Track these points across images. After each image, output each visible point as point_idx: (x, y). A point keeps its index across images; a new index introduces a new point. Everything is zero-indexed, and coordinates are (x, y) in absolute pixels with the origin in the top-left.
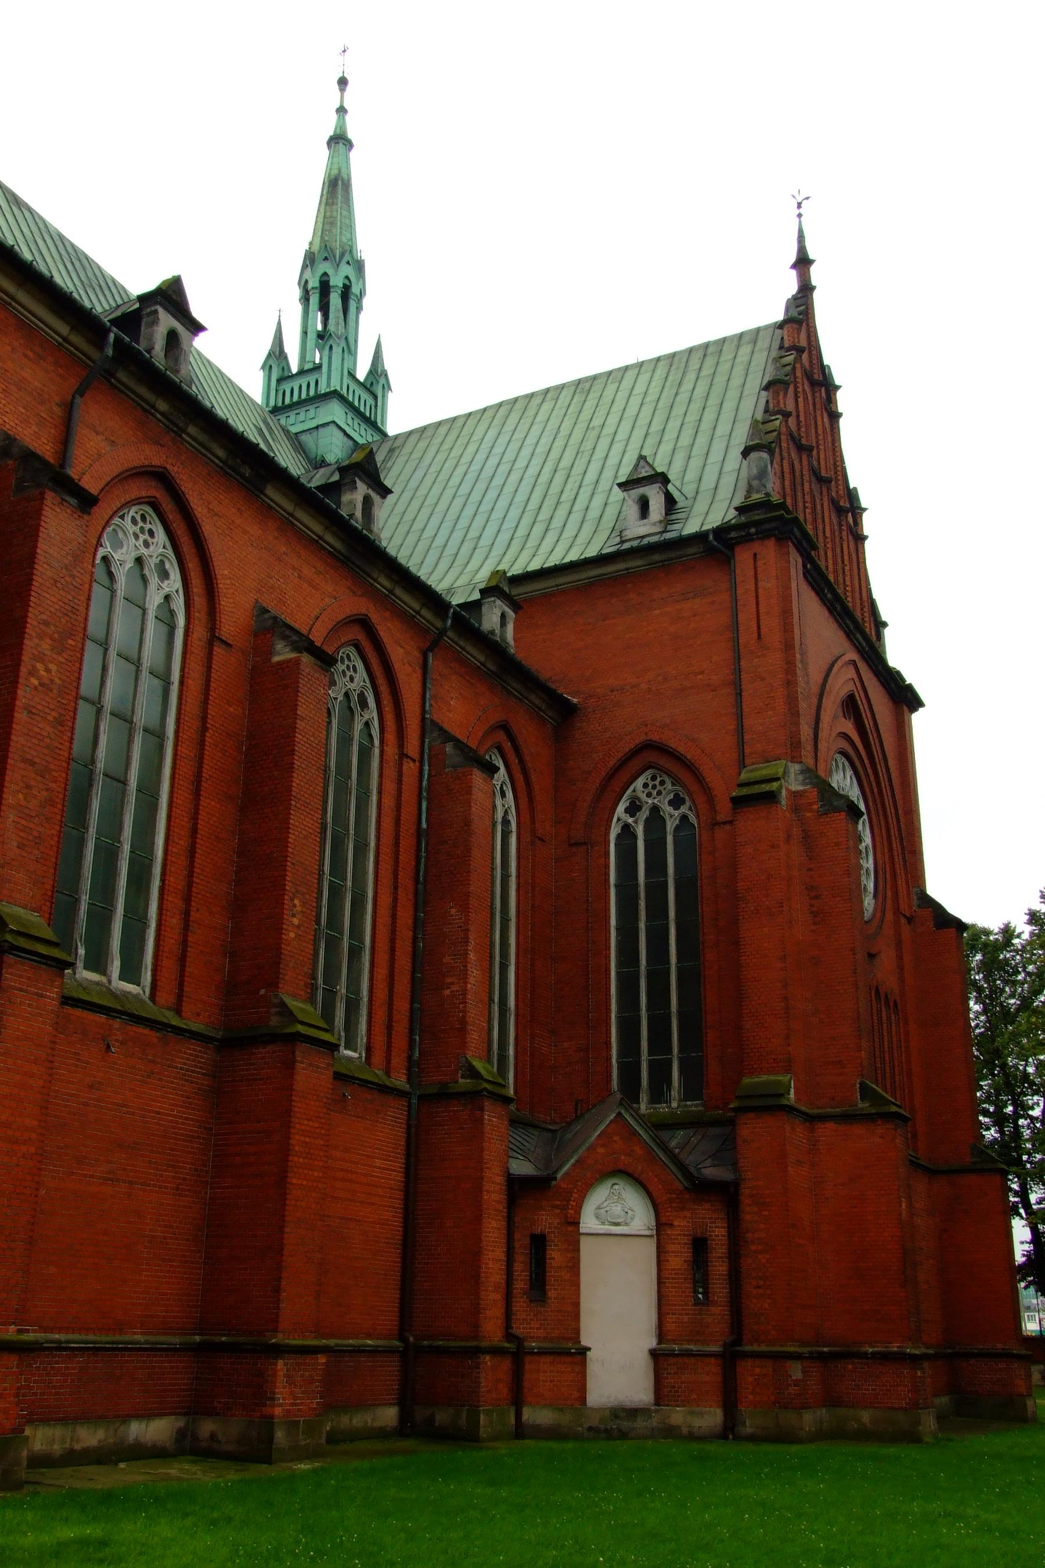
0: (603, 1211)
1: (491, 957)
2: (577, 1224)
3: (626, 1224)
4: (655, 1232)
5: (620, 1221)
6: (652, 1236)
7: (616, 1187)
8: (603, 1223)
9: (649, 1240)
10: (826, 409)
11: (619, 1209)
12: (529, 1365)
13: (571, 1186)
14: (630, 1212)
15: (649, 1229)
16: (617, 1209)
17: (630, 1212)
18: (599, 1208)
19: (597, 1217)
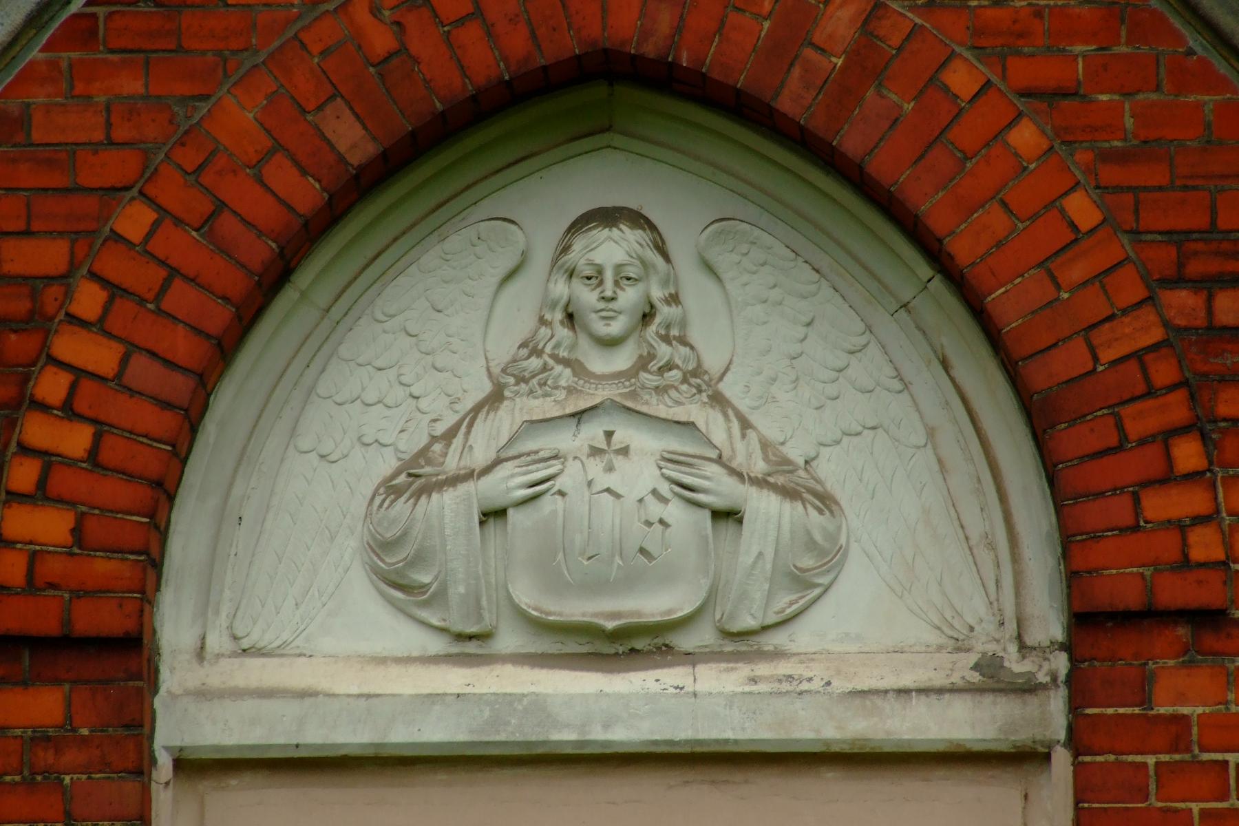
0: (451, 509)
1: (155, 441)
2: (121, 657)
3: (741, 643)
4: (1051, 716)
5: (654, 605)
6: (1024, 758)
7: (612, 248)
8: (470, 645)
9: (996, 796)
10: (40, 590)
11: (640, 474)
12: (127, 380)
13: (48, 255)
14: (763, 508)
15: (992, 680)
16: (617, 485)
17: (763, 508)
18: (416, 479)
19: (401, 577)
